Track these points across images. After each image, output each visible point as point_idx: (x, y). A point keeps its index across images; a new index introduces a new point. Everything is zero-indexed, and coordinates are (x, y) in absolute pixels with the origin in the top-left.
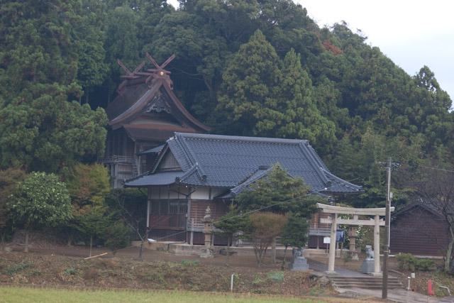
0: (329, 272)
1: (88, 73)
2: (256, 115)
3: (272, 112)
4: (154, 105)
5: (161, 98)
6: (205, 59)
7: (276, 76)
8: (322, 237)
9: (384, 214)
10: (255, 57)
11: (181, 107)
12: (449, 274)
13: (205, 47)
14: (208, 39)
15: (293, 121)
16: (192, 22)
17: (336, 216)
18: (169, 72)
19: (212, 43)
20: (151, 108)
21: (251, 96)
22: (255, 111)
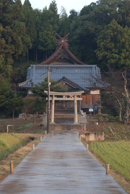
0: (75, 123)
1: (46, 45)
2: (107, 57)
3: (114, 55)
4: (60, 56)
5: (63, 52)
6: (96, 34)
7: (118, 39)
8: (88, 109)
9: (65, 96)
10: (109, 31)
11: (72, 55)
12: (121, 123)
13: (96, 29)
14: (98, 25)
15: (124, 59)
16: (92, 18)
17: (54, 96)
18: (67, 40)
19: (99, 27)
20: (59, 57)
21: (107, 49)
22: (107, 55)
